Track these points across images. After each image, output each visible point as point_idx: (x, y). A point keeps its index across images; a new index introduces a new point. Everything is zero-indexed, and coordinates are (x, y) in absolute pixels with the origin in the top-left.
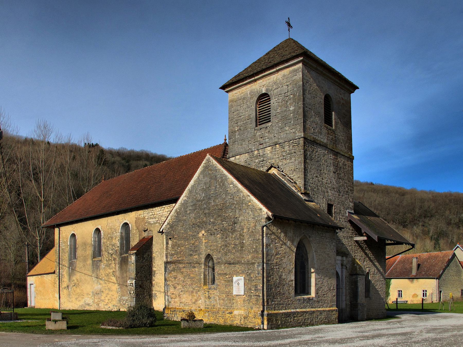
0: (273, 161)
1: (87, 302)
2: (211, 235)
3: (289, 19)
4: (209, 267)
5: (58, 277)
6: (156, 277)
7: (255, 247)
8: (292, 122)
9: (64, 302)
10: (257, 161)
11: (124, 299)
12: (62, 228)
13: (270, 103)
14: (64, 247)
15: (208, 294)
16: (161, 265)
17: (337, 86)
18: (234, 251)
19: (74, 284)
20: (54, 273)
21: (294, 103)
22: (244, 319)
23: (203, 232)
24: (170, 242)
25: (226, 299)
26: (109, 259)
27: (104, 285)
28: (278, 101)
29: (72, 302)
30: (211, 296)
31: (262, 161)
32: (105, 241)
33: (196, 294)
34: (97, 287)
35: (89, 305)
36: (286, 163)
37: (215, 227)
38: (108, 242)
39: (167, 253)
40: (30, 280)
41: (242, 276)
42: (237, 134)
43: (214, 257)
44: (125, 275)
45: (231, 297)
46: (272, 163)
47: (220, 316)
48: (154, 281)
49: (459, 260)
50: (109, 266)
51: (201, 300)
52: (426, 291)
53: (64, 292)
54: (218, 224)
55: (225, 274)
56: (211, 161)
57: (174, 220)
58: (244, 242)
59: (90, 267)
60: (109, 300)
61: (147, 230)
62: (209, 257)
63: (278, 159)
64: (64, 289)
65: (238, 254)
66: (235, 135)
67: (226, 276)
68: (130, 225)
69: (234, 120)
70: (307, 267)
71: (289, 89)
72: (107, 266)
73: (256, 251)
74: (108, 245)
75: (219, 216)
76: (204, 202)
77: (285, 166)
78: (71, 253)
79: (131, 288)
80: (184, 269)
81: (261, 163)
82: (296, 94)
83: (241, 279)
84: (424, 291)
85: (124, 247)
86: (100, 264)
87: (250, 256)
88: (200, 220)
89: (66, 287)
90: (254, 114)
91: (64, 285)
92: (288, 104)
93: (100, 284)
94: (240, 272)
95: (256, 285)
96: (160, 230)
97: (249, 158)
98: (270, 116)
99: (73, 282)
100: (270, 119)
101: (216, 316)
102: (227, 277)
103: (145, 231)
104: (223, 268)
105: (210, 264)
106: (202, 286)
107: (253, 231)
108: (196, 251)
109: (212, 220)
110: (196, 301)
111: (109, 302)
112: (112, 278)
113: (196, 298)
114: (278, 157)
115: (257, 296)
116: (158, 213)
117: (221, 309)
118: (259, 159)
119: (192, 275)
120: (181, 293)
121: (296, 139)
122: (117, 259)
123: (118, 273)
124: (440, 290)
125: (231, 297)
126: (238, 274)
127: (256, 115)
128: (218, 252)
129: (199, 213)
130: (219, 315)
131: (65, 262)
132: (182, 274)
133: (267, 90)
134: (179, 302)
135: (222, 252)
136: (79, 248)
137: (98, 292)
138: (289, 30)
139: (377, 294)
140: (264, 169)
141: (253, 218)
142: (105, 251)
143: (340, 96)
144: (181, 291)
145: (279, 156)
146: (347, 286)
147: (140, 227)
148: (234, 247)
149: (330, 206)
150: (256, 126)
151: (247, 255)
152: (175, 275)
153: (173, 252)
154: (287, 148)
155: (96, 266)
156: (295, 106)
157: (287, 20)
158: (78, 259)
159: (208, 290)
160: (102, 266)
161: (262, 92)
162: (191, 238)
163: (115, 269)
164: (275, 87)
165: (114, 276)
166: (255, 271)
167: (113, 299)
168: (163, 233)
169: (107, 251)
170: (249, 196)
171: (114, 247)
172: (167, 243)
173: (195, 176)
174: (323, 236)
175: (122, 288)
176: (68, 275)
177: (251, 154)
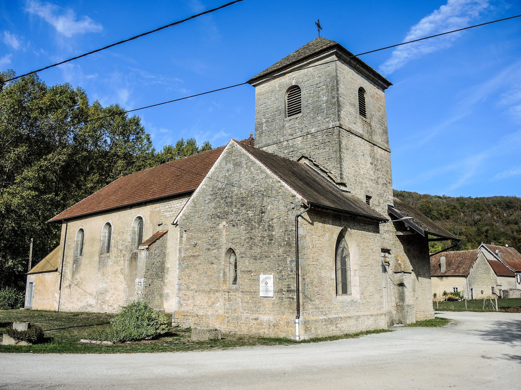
0: (305, 151)
1: (89, 303)
2: (234, 226)
3: (319, 21)
4: (230, 263)
5: (60, 275)
6: (170, 275)
7: (286, 239)
8: (325, 112)
9: (65, 303)
10: (286, 151)
11: (131, 300)
12: (70, 224)
13: (300, 95)
14: (70, 243)
15: (228, 296)
16: (176, 261)
17: (371, 80)
18: (261, 244)
19: (77, 283)
20: (56, 270)
21: (327, 93)
22: (273, 327)
23: (224, 223)
24: (185, 235)
25: (251, 301)
26: (118, 256)
27: (110, 284)
28: (310, 92)
29: (73, 302)
30: (231, 298)
31: (292, 152)
32: (115, 236)
33: (213, 296)
34: (102, 286)
35: (91, 306)
36: (318, 153)
37: (238, 217)
38: (119, 238)
39: (181, 248)
40: (30, 278)
41: (271, 274)
42: (264, 125)
43: (237, 251)
44: (134, 273)
45: (256, 299)
46: (303, 153)
47: (243, 323)
48: (167, 279)
49: (487, 259)
50: (117, 262)
51: (219, 303)
52: (457, 289)
53: (65, 292)
54: (242, 214)
55: (250, 271)
56: (235, 146)
57: (191, 211)
58: (274, 233)
59: (96, 264)
60: (114, 300)
61: (162, 224)
62: (231, 251)
63: (309, 149)
64: (65, 288)
65: (265, 248)
66: (262, 127)
67: (251, 273)
68: (144, 219)
69: (261, 112)
70: (349, 263)
71: (321, 80)
72: (115, 263)
73: (289, 244)
74: (118, 241)
75: (243, 205)
76: (225, 190)
77: (317, 156)
78: (77, 249)
79: (139, 287)
80: (200, 265)
81: (290, 153)
82: (329, 84)
83: (270, 278)
84: (454, 289)
85: (135, 242)
86: (107, 261)
87: (280, 250)
88: (221, 210)
89: (68, 286)
90: (283, 106)
91: (66, 283)
92: (320, 94)
93: (106, 283)
94: (268, 269)
95: (288, 285)
96: (173, 222)
97: (277, 149)
98: (301, 107)
99: (76, 281)
100: (301, 109)
101: (238, 322)
102: (252, 274)
103: (159, 225)
104: (247, 264)
105: (232, 259)
106: (221, 286)
107: (284, 221)
108: (215, 244)
109: (234, 210)
110: (213, 303)
111: (114, 303)
112: (119, 275)
113: (213, 300)
114: (310, 146)
115: (290, 298)
116: (175, 206)
117: (244, 313)
118: (289, 150)
119: (209, 273)
120: (195, 294)
121: (330, 129)
122: (127, 255)
123: (127, 271)
124: (471, 288)
125: (256, 299)
126: (266, 271)
127: (285, 109)
128: (241, 246)
129: (220, 202)
130: (242, 322)
131: (69, 260)
132: (198, 271)
133: (297, 82)
134: (192, 305)
135: (247, 245)
136: (86, 244)
137: (102, 292)
138: (319, 31)
139: (423, 294)
140: (295, 159)
141: (284, 207)
142: (115, 246)
143: (374, 90)
144: (195, 291)
145: (311, 146)
146: (391, 285)
147: (155, 221)
148: (261, 240)
149: (368, 198)
150: (286, 117)
151: (277, 248)
152: (188, 273)
153: (188, 246)
154: (320, 138)
155: (102, 263)
156: (328, 96)
157: (317, 22)
158: (84, 256)
159: (228, 291)
160: (110, 262)
161: (292, 84)
162: (209, 230)
163: (124, 266)
164: (305, 79)
165: (122, 273)
166: (287, 268)
167: (119, 300)
168: (178, 225)
169: (116, 246)
170: (280, 182)
171: (124, 243)
172: (181, 237)
173: (216, 163)
174: (365, 229)
175: (130, 288)
176: (71, 273)
177: (280, 145)
